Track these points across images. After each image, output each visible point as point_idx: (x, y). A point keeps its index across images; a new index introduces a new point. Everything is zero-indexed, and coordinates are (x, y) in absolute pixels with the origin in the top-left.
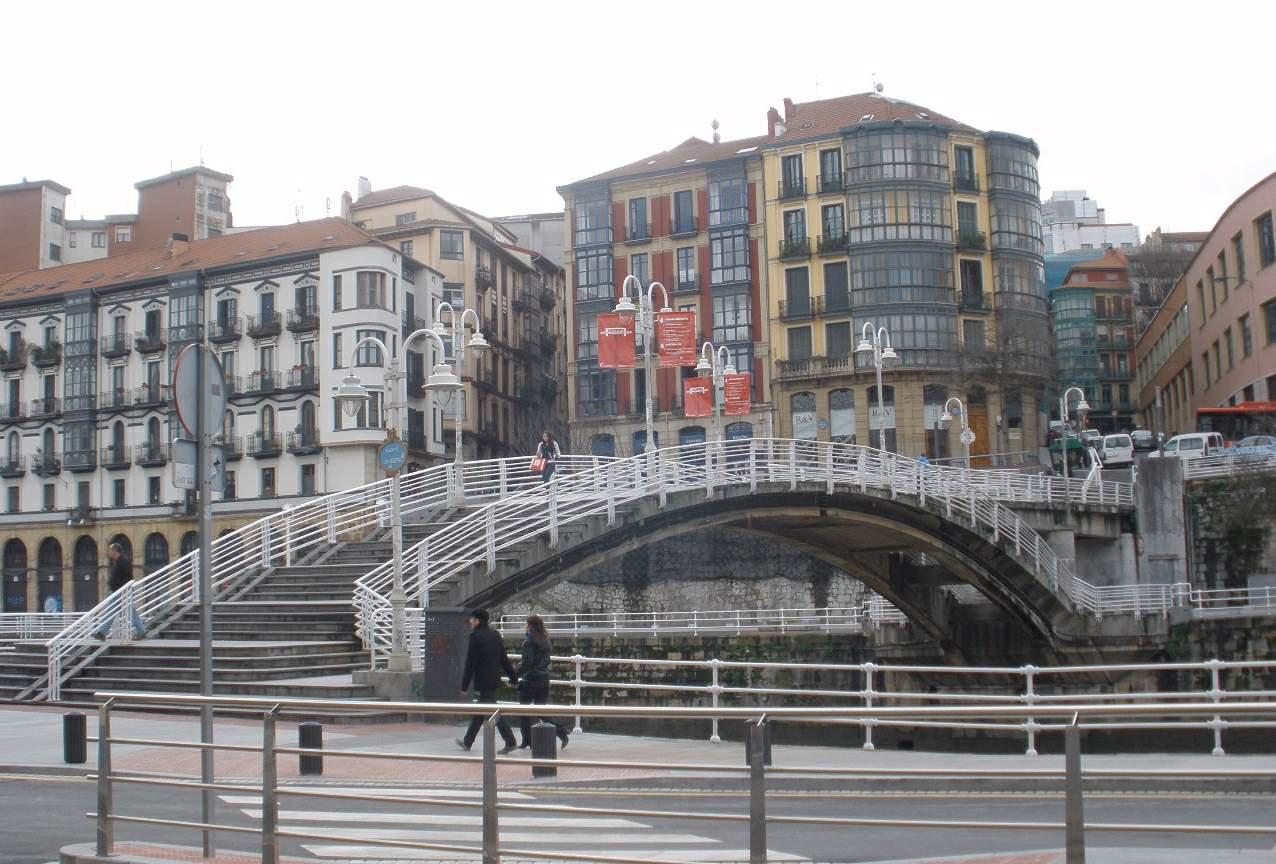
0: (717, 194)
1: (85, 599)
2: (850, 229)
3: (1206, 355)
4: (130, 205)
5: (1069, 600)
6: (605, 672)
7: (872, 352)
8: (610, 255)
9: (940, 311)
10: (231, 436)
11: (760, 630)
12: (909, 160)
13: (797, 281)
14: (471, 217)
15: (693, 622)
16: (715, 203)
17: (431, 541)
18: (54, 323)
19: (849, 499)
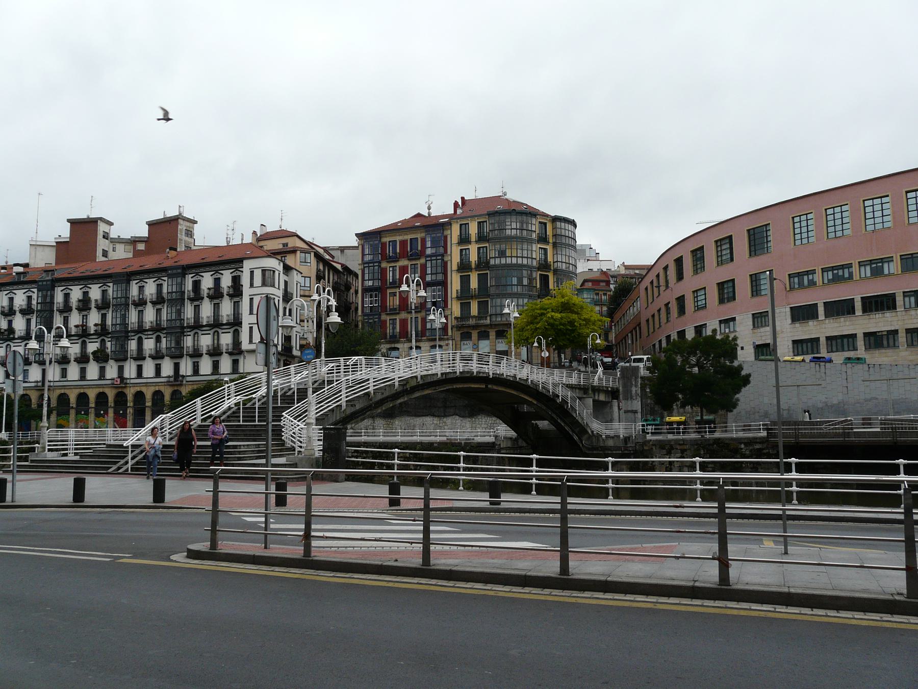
0: (430, 240)
1: (139, 423)
2: (490, 258)
3: (648, 321)
4: (144, 232)
5: (591, 429)
6: (475, 460)
7: (510, 314)
8: (379, 266)
9: (530, 297)
10: (160, 347)
11: (447, 439)
12: (518, 227)
13: (465, 281)
14: (313, 246)
15: (399, 435)
16: (429, 244)
17: (318, 395)
18: (107, 288)
19: (499, 380)
